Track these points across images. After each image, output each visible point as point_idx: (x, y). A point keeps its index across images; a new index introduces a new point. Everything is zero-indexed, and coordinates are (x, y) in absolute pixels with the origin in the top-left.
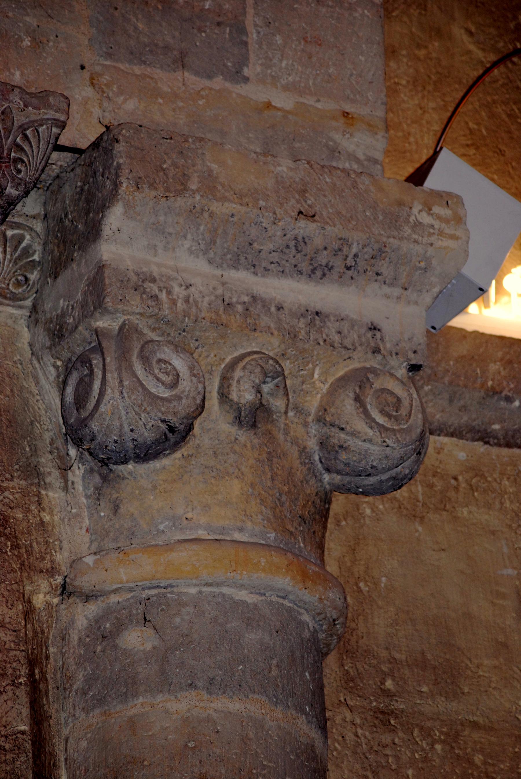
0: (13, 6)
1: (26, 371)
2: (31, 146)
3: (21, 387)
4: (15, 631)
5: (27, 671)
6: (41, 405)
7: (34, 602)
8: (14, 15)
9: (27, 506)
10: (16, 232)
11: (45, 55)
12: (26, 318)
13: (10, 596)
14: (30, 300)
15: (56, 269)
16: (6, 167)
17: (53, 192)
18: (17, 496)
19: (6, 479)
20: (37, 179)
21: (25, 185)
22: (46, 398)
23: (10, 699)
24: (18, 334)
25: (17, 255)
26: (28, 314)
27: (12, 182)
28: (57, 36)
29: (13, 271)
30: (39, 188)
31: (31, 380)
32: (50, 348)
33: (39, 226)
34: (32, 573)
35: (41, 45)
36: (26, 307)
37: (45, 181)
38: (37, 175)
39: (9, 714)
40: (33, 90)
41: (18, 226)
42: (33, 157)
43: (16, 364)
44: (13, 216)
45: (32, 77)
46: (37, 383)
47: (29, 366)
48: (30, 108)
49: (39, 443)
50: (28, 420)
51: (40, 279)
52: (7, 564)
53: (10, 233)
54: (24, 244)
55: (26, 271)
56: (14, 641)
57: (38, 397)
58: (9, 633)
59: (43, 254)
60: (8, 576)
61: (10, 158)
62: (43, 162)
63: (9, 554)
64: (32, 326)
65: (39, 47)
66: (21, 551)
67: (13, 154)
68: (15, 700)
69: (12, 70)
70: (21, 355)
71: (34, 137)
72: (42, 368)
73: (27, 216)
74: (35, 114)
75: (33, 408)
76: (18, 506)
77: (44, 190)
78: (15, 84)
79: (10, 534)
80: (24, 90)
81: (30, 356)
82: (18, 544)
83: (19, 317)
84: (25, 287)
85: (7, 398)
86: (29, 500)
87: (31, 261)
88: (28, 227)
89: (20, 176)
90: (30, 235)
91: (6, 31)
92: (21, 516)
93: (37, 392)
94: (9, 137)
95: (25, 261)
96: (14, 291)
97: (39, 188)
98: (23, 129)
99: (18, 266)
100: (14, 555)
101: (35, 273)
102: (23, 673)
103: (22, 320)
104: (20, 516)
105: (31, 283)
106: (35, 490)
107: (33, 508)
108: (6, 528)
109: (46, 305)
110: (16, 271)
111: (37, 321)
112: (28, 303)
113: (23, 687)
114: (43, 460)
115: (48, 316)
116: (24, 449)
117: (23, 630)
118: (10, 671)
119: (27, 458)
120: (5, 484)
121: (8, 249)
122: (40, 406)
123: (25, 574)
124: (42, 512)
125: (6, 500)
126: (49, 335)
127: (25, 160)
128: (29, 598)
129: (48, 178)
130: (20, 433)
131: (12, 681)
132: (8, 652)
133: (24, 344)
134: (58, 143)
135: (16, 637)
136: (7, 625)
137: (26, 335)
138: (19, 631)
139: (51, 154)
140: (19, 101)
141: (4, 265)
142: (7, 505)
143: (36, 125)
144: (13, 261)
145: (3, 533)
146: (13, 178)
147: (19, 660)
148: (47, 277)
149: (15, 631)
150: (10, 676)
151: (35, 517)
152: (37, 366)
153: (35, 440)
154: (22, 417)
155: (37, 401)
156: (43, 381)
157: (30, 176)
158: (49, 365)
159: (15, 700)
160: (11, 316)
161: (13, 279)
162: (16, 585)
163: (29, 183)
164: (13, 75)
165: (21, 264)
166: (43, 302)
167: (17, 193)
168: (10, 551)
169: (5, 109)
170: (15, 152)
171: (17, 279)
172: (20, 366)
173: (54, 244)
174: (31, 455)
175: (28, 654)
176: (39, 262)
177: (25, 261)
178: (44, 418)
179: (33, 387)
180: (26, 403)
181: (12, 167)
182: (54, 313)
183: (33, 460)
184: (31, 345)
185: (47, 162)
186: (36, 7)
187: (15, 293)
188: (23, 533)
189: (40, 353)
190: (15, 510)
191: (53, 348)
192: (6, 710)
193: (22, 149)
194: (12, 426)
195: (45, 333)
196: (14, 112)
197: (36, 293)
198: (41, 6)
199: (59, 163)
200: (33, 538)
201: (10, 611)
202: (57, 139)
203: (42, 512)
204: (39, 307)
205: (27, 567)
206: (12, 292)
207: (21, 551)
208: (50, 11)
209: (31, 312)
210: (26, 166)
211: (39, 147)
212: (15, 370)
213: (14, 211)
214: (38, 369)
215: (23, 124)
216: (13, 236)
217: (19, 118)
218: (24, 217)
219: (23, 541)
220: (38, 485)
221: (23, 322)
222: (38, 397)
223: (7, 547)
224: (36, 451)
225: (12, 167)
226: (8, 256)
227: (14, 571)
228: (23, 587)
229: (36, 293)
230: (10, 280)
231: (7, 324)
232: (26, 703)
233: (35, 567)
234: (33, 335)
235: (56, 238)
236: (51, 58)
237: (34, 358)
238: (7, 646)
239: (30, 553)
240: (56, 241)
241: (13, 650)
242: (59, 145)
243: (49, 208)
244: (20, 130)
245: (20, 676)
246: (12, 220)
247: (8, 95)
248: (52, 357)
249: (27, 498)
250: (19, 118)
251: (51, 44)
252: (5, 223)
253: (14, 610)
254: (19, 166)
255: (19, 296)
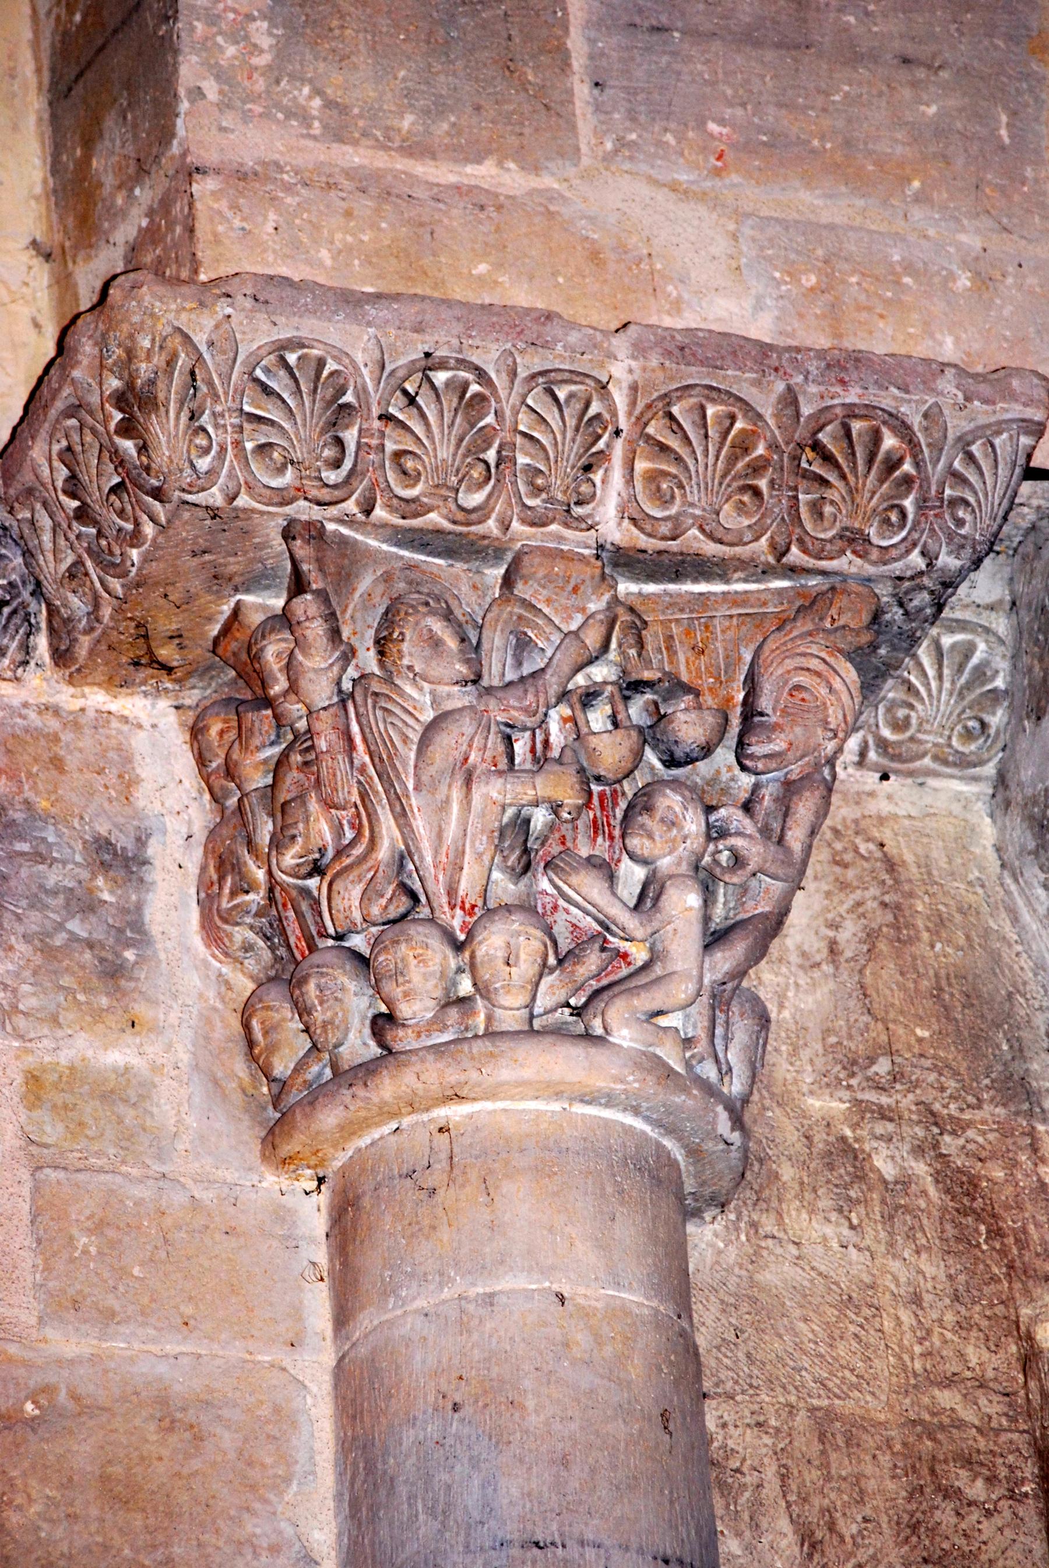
0: (937, 216)
1: (992, 900)
2: (982, 474)
3: (986, 930)
4: (1007, 1395)
5: (1036, 1471)
6: (1024, 961)
7: (1038, 1337)
8: (938, 233)
9: (1011, 1155)
10: (959, 637)
11: (998, 302)
12: (988, 798)
13: (990, 1327)
14: (991, 764)
15: (1039, 701)
16: (936, 515)
17: (1025, 558)
18: (991, 1136)
19: (969, 1106)
20: (996, 535)
21: (974, 548)
22: (1034, 947)
23: (1008, 1525)
24: (973, 830)
25: (963, 680)
26: (990, 791)
27: (948, 544)
28: (1020, 266)
29: (957, 711)
30: (998, 553)
31: (1004, 915)
32: (1036, 853)
33: (1001, 624)
34: (1031, 1283)
35: (990, 283)
36: (987, 778)
37: (1009, 538)
38: (995, 527)
39: (1009, 1553)
40: (979, 369)
41: (962, 625)
42: (986, 495)
43: (973, 886)
44: (952, 608)
45: (976, 346)
46: (1015, 920)
47: (998, 888)
48: (976, 403)
49: (1024, 1034)
50: (1003, 992)
51: (1008, 723)
52: (981, 1266)
53: (947, 641)
54: (975, 660)
55: (981, 710)
56: (1006, 1415)
57: (1019, 948)
58: (996, 1398)
59: (1012, 676)
60: (986, 1290)
61: (942, 500)
62: (1005, 503)
63: (985, 1247)
64: (998, 813)
65: (987, 288)
66: (1006, 1241)
67: (948, 492)
68: (1018, 1526)
69: (938, 336)
70: (982, 869)
71: (986, 456)
72: (1022, 891)
73: (978, 606)
74: (986, 413)
75: (1011, 968)
76: (993, 1156)
77: (1008, 555)
78: (946, 361)
79: (983, 1210)
80: (963, 370)
81: (998, 870)
82: (1000, 1229)
83: (974, 799)
84: (981, 741)
85: (960, 953)
86: (1014, 1143)
87: (990, 691)
88: (981, 626)
89: (963, 532)
90: (987, 641)
91: (925, 263)
92: (1002, 1174)
93: (1016, 937)
94: (938, 460)
95: (978, 691)
96: (961, 749)
97: (998, 553)
98: (964, 443)
99: (965, 703)
100: (994, 1249)
101: (1000, 712)
102: (1028, 1475)
103: (980, 804)
104: (999, 1174)
105: (992, 731)
106: (1025, 1123)
107: (1024, 1158)
108: (974, 1199)
109: (1023, 773)
110: (963, 711)
111: (1007, 804)
112: (990, 770)
113: (1031, 1502)
114: (1035, 1066)
115: (1029, 791)
116: (998, 1046)
117: (1022, 1393)
118: (1003, 1472)
119: (1005, 1064)
120: (966, 1116)
121: (946, 672)
122: (1023, 964)
123: (1017, 1286)
124: (1040, 1165)
125: (971, 1147)
126: (1032, 828)
127: (971, 500)
128: (1028, 1331)
129: (1014, 532)
130: (989, 1017)
131: (1009, 1490)
132: (997, 1436)
133: (985, 848)
134: (1032, 464)
135: (1010, 1405)
136: (991, 1384)
137: (988, 830)
138: (1015, 1394)
139: (1019, 485)
140: (955, 391)
141: (939, 701)
142: (974, 1155)
143: (989, 432)
144: (956, 693)
145: (971, 1208)
146: (950, 536)
147: (1018, 1450)
148: (1021, 720)
149: (1007, 1395)
150: (1004, 1481)
151: (1028, 1176)
152: (1013, 887)
153: (1019, 1028)
154: (990, 986)
155: (1018, 954)
156: (1026, 917)
157: (982, 529)
158: (1036, 884)
159: (1018, 1526)
160: (958, 797)
161: (959, 728)
162: (1001, 1307)
163: (980, 543)
164: (941, 344)
165: (971, 697)
166: (1017, 767)
167: (958, 563)
168: (986, 1242)
169: (930, 407)
170: (951, 487)
171: (966, 727)
172: (980, 891)
173: (1033, 656)
174: (1013, 1059)
175: (1035, 1439)
176: (1006, 692)
177: (978, 691)
178: (1032, 986)
179: (1007, 929)
180: (996, 958)
181: (947, 517)
182: (1040, 786)
183: (1018, 1068)
184: (998, 850)
185: (1012, 503)
186: (978, 214)
187: (963, 753)
188: (1007, 1207)
189: (1017, 863)
190: (989, 1164)
191: (1042, 852)
192: (1003, 1546)
193: (964, 481)
194: (973, 1005)
195: (1024, 826)
196: (946, 412)
197: (1003, 750)
198: (988, 212)
199: (1035, 502)
200: (1027, 1215)
201: (994, 1357)
202: (1029, 457)
203: (1040, 1165)
204: (1009, 775)
205: (1020, 1272)
206: (957, 752)
207: (1006, 1241)
208: (1005, 220)
209: (995, 787)
210: (973, 511)
211: (996, 474)
212: (972, 898)
213: (953, 599)
214: (1016, 894)
215: (966, 434)
216: (954, 646)
217: (955, 422)
218: (974, 608)
219: (1008, 1224)
220: (1030, 1114)
221: (981, 808)
222: (1019, 948)
223: (980, 1235)
224: (1021, 1050)
225: (947, 517)
226: (947, 685)
227: (994, 1279)
228: (1016, 1309)
229: (1003, 750)
230: (952, 730)
231: (951, 813)
232: (1040, 1531)
233: (1035, 1271)
234: (1002, 830)
235: (1035, 645)
236: (1011, 308)
237: (1006, 873)
238: (994, 1424)
239: (1023, 1244)
240: (1036, 649)
241: (1005, 1430)
242: (1034, 469)
243: (1020, 588)
244: (960, 445)
245: (1023, 1481)
246: (951, 616)
247: (934, 381)
248: (1041, 868)
249: (1010, 1141)
250: (955, 422)
251: (1010, 280)
252: (938, 623)
253: (1001, 1354)
254: (961, 514)
255: (973, 758)
